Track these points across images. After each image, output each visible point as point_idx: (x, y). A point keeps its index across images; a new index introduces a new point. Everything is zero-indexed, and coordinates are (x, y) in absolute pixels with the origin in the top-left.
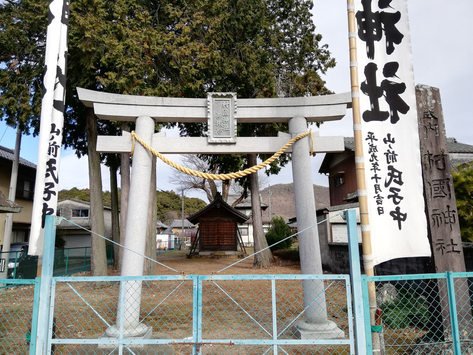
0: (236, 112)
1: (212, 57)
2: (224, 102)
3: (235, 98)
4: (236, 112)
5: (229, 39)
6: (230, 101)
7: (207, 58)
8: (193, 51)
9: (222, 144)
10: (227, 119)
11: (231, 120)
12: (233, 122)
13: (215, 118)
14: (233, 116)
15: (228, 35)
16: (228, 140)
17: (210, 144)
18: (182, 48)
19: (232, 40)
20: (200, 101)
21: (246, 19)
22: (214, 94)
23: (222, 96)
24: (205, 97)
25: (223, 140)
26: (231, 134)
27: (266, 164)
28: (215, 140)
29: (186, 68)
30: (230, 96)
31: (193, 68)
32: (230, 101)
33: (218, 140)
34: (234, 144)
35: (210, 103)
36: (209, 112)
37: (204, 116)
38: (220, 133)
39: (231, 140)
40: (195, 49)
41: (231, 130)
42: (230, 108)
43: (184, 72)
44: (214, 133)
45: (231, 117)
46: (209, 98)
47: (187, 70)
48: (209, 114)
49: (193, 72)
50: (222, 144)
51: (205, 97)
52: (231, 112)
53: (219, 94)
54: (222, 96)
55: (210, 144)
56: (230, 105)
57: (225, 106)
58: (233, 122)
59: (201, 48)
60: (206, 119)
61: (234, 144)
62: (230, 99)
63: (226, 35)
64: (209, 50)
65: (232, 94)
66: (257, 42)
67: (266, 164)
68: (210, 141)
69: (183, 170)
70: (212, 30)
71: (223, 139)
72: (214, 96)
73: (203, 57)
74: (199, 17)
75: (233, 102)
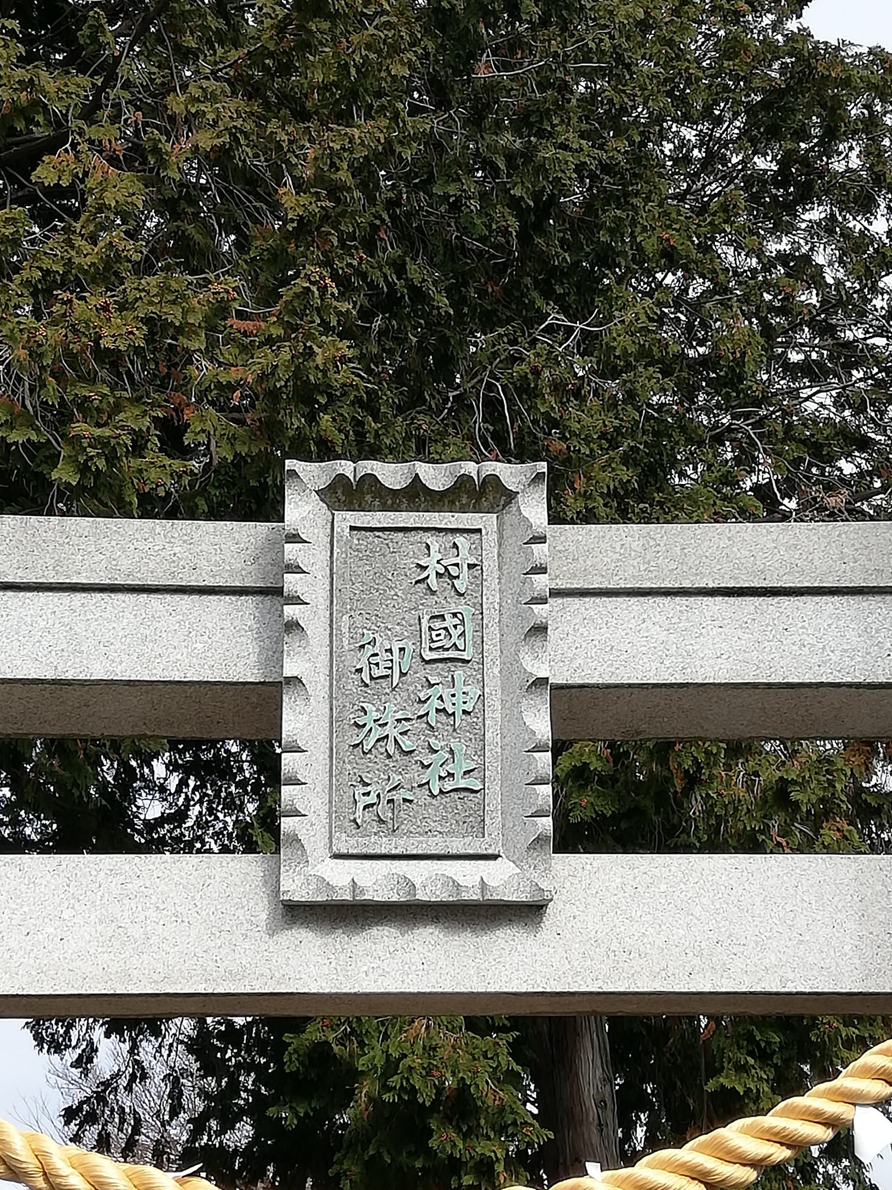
0: (540, 630)
1: (298, 374)
2: (432, 544)
3: (534, 509)
4: (540, 630)
5: (418, 294)
6: (490, 539)
7: (262, 378)
8: (155, 326)
9: (409, 913)
10: (460, 691)
11: (494, 702)
12: (512, 716)
13: (352, 684)
14: (511, 666)
15: (411, 267)
16: (469, 880)
17: (298, 913)
18: (86, 307)
19: (443, 301)
20: (220, 546)
21: (541, 169)
22: (341, 478)
23: (416, 495)
24: (257, 499)
25: (428, 881)
26: (494, 822)
27: (854, 1099)
28: (342, 879)
29: (101, 443)
30: (489, 496)
31: (153, 454)
32: (490, 539)
33: (376, 882)
34: (529, 912)
35: (312, 556)
36: (293, 626)
37: (241, 666)
38: (388, 813)
39: (502, 879)
40: (174, 315)
41: (494, 791)
42: (491, 598)
43: (84, 469)
44: (339, 817)
45: (493, 671)
46: (301, 508)
47: (112, 459)
48: (291, 642)
49: (153, 474)
50: (409, 913)
51: (257, 499)
52: (492, 632)
53: (391, 474)
54: (416, 495)
55: (298, 913)
56: (490, 564)
57: (444, 574)
58: (512, 716)
59: (221, 309)
60: (261, 701)
61: (529, 912)
62: (487, 521)
63: (400, 269)
64: (277, 331)
65: (510, 474)
66: (615, 326)
67: (854, 1099)
68: (296, 887)
69: (30, 1163)
70: (304, 199)
71: (417, 871)
72: (341, 495)
73: (234, 375)
74: (212, 112)
75: (514, 541)
